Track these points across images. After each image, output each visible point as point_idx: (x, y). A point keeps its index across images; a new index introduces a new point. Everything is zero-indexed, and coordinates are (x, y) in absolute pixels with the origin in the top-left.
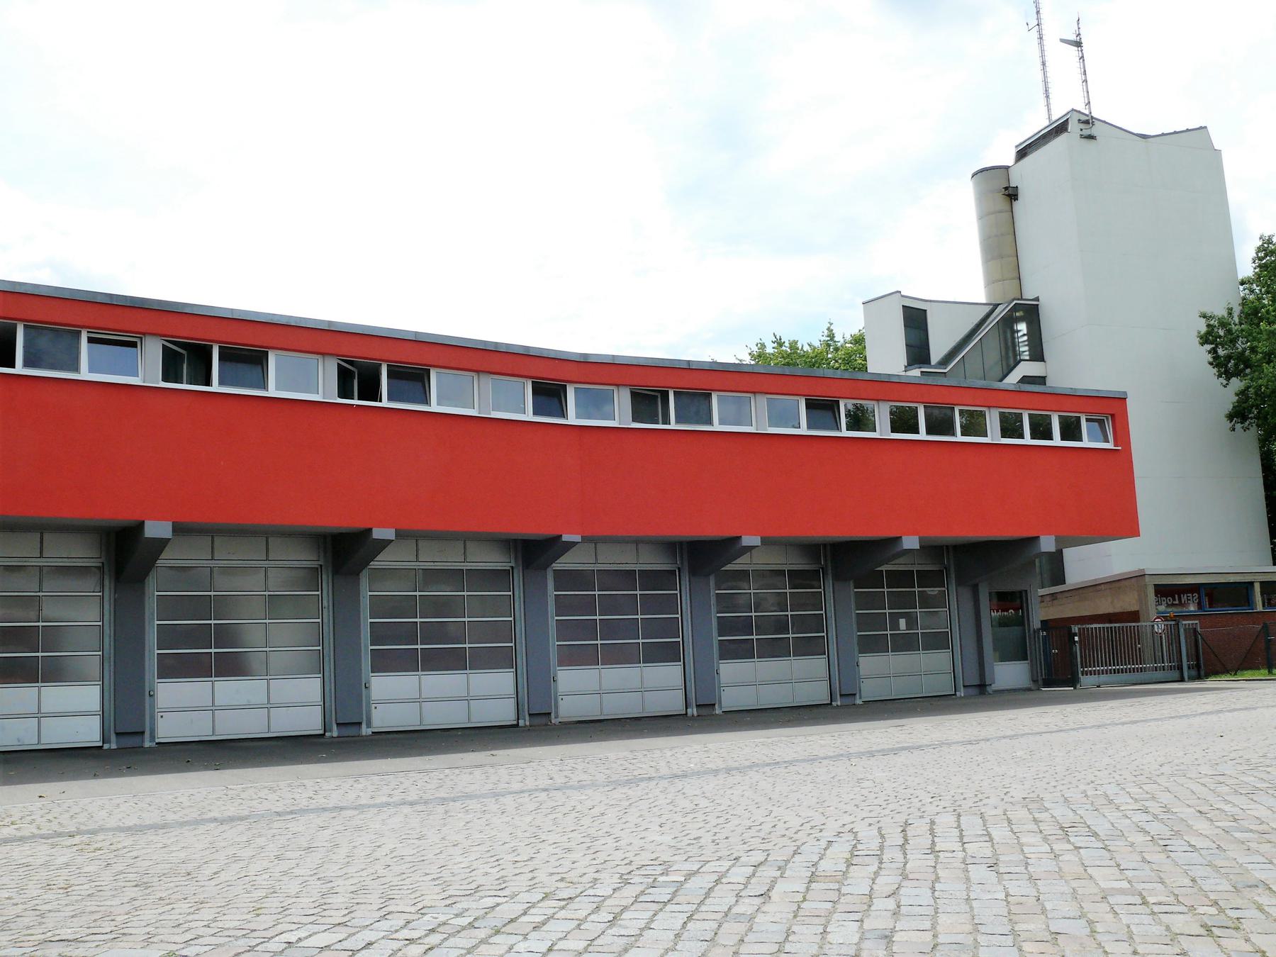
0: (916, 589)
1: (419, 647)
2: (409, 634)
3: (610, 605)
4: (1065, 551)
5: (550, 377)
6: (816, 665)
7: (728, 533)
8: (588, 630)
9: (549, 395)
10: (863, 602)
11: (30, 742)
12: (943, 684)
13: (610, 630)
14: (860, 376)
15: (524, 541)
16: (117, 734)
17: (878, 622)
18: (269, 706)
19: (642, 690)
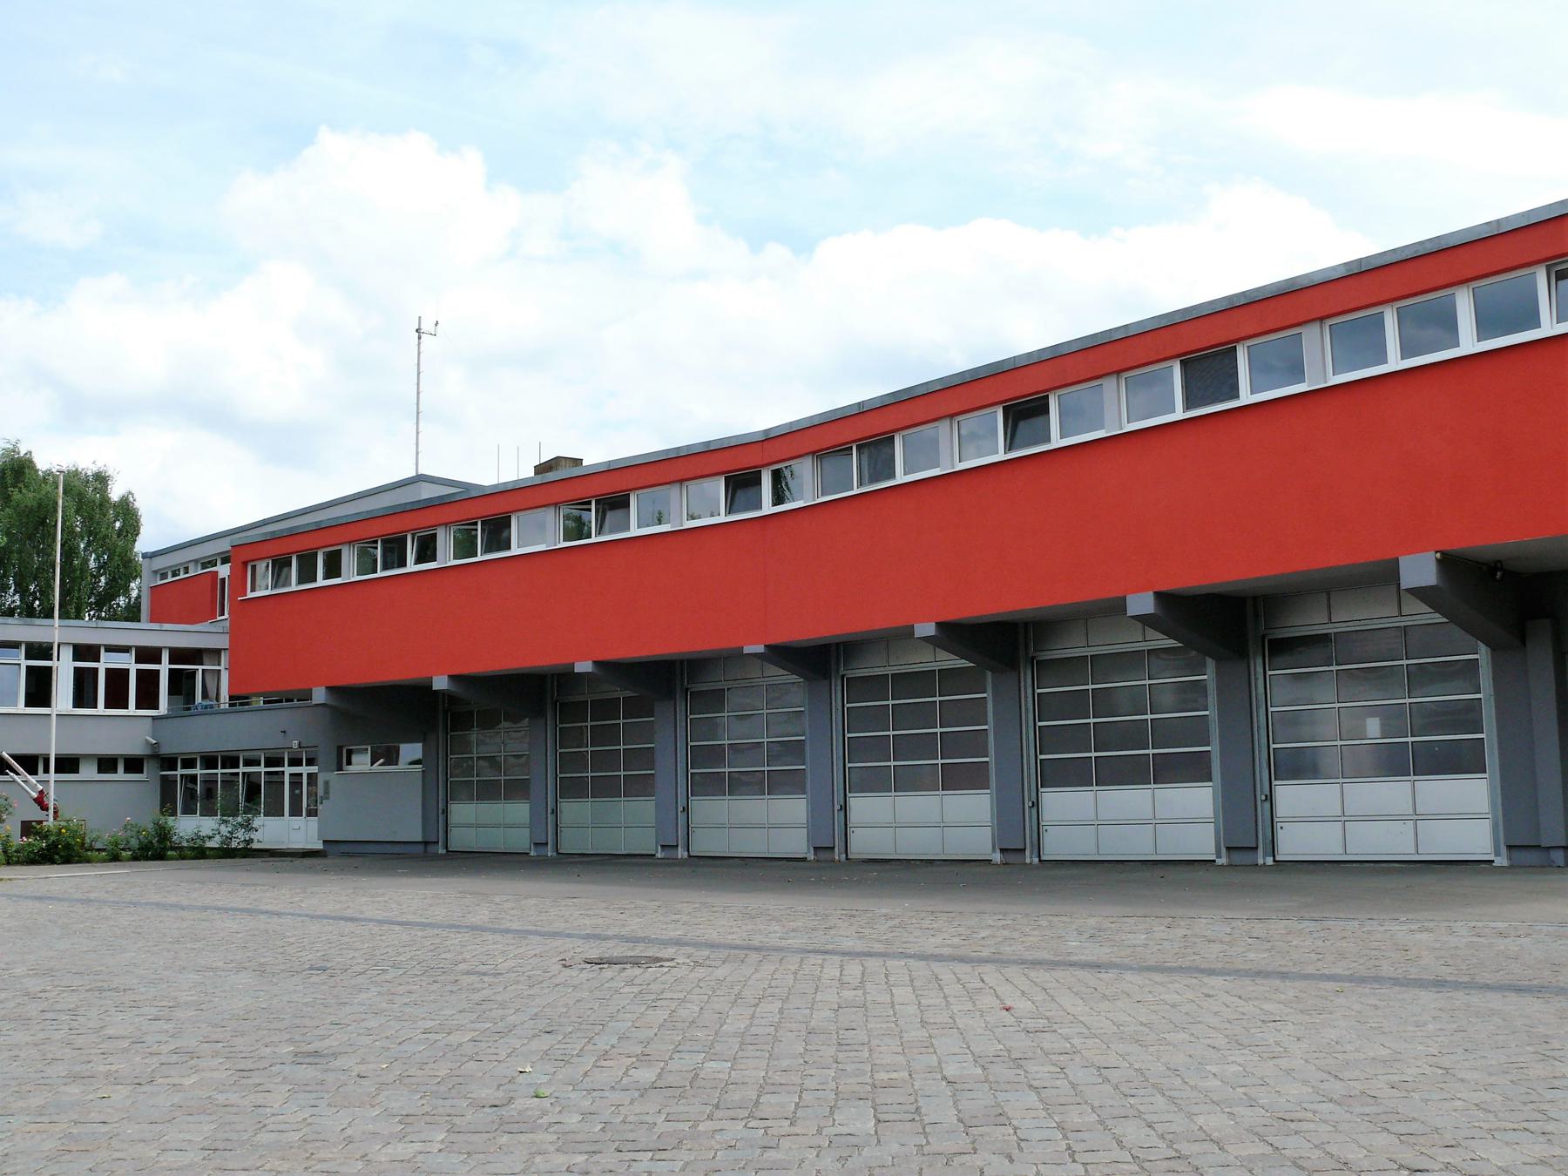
0: (621, 721)
1: (1151, 751)
2: (1076, 737)
3: (903, 716)
4: (1129, 598)
5: (741, 466)
6: (519, 810)
7: (899, 621)
8: (878, 747)
9: (1025, 412)
10: (565, 738)
11: (1333, 851)
12: (1202, 842)
13: (904, 747)
14: (576, 472)
15: (689, 661)
16: (1510, 847)
17: (577, 761)
18: (1344, 819)
19: (1155, 823)
